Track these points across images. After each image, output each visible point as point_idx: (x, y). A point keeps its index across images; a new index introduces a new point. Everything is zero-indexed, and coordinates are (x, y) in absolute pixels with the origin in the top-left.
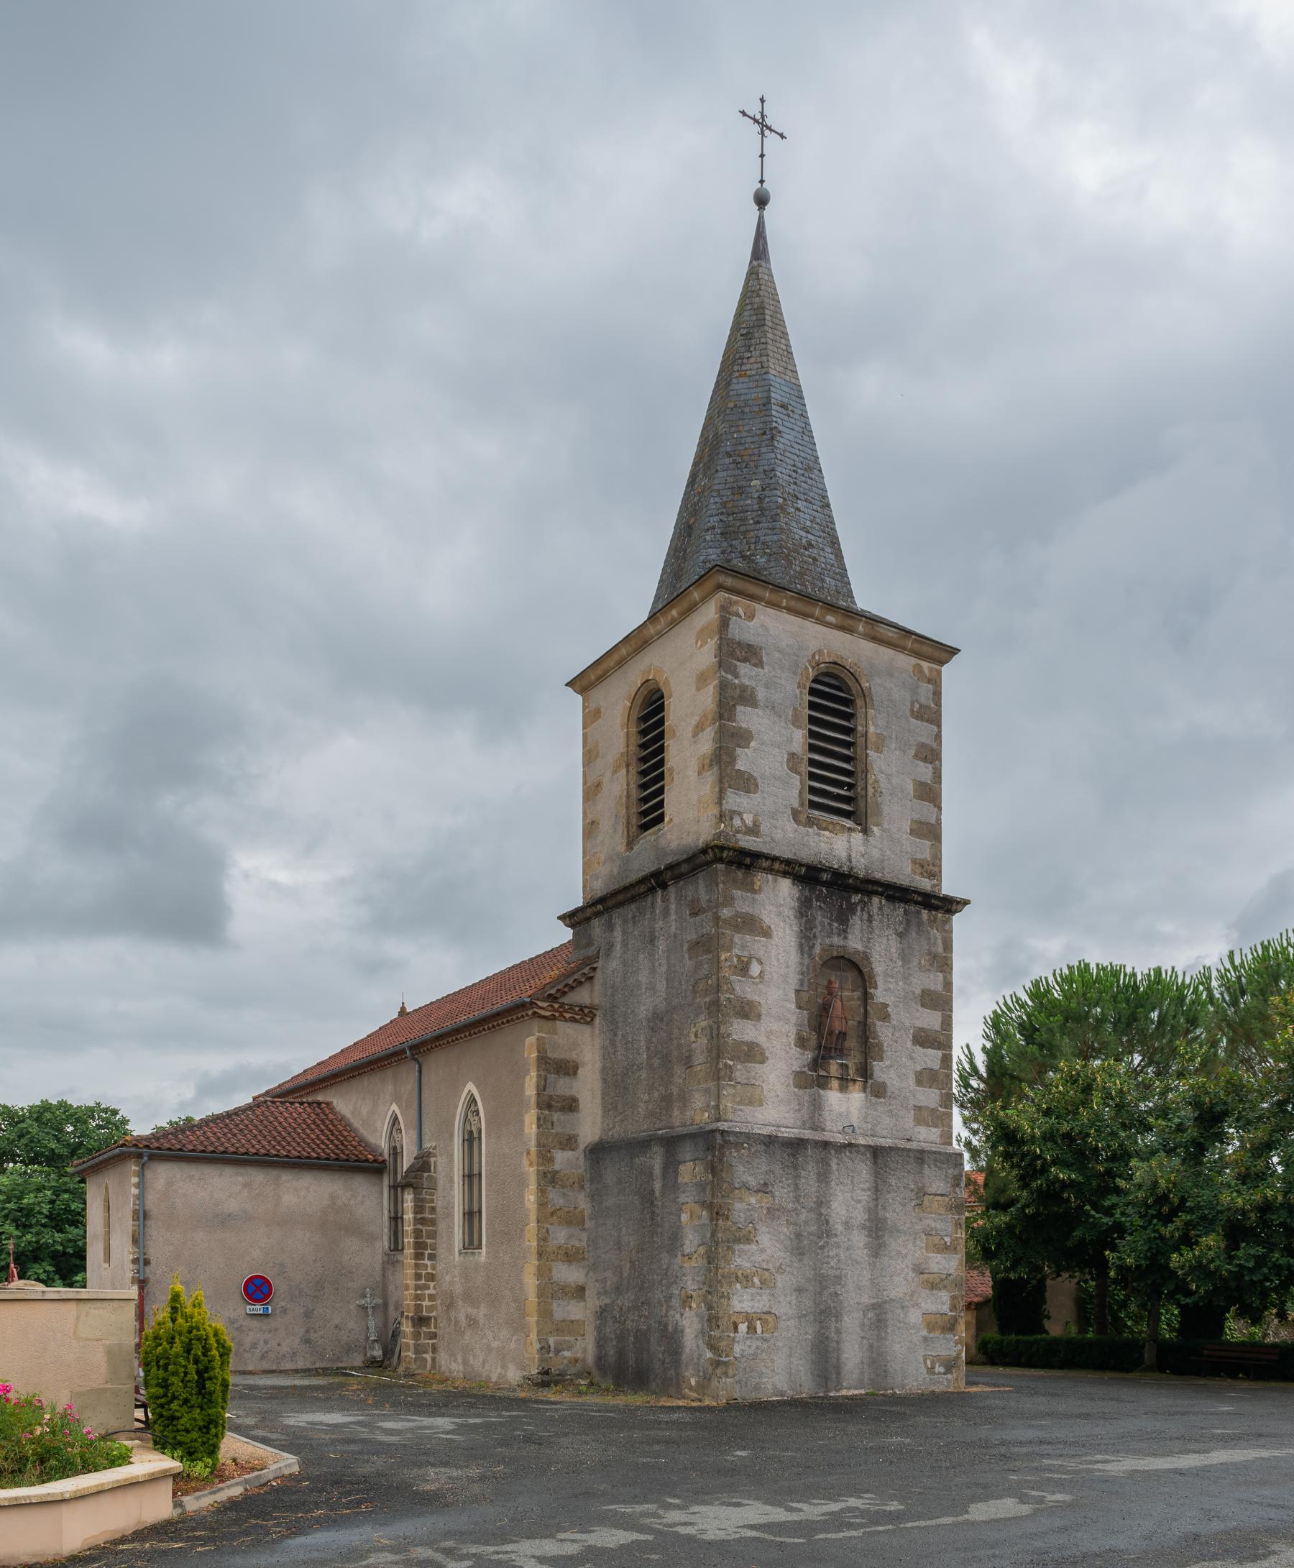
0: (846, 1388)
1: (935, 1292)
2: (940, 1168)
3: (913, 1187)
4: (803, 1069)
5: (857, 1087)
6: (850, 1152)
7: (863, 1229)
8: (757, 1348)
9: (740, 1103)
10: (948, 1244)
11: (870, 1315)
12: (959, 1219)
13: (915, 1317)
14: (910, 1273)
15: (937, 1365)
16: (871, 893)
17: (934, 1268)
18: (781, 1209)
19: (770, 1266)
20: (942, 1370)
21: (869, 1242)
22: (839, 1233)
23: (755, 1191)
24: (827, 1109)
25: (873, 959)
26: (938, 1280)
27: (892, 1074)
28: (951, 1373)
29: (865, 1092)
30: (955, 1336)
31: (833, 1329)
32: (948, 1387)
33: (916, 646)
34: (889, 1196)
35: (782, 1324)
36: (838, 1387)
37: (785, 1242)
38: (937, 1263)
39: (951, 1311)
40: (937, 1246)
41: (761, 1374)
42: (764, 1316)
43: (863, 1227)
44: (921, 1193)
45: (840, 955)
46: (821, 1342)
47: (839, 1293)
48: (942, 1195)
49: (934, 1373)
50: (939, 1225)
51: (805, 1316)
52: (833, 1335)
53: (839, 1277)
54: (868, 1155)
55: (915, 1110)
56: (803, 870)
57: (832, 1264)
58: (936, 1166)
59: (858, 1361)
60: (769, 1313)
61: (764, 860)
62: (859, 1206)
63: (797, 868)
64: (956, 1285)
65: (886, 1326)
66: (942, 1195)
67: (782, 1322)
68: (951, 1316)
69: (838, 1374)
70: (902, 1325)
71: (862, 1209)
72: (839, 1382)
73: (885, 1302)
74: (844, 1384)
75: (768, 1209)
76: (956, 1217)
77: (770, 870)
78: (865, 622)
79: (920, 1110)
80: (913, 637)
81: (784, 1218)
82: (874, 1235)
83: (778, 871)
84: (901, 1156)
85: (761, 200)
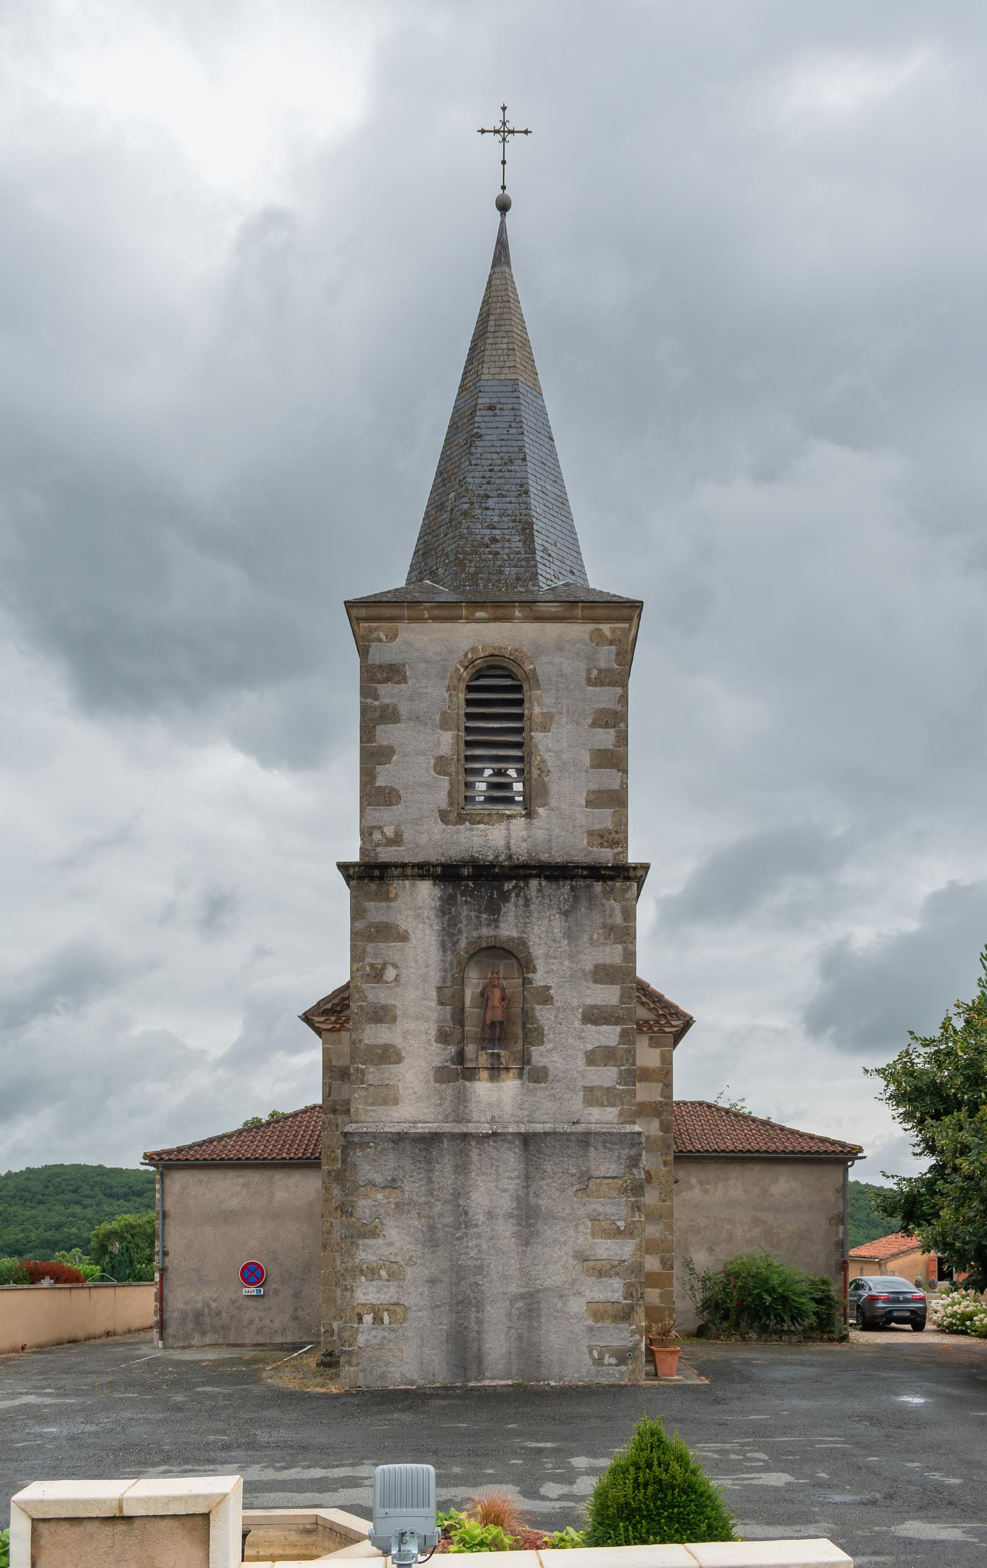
0: (489, 1378)
2: (610, 1149)
3: (574, 1171)
7: (512, 1217)
13: (576, 1306)
14: (571, 1260)
15: (607, 1356)
16: (527, 878)
20: (613, 1361)
24: (474, 1099)
26: (608, 1267)
28: (626, 1364)
30: (630, 1325)
36: (480, 1375)
38: (607, 1249)
39: (625, 1299)
48: (613, 1178)
50: (610, 1209)
56: (439, 870)
59: (504, 1351)
61: (393, 868)
62: (505, 1195)
63: (431, 869)
64: (632, 1272)
65: (540, 1316)
66: (613, 1178)
68: (626, 1305)
69: (480, 1364)
70: (560, 1314)
73: (539, 1291)
77: (404, 877)
78: (520, 606)
85: (503, 206)
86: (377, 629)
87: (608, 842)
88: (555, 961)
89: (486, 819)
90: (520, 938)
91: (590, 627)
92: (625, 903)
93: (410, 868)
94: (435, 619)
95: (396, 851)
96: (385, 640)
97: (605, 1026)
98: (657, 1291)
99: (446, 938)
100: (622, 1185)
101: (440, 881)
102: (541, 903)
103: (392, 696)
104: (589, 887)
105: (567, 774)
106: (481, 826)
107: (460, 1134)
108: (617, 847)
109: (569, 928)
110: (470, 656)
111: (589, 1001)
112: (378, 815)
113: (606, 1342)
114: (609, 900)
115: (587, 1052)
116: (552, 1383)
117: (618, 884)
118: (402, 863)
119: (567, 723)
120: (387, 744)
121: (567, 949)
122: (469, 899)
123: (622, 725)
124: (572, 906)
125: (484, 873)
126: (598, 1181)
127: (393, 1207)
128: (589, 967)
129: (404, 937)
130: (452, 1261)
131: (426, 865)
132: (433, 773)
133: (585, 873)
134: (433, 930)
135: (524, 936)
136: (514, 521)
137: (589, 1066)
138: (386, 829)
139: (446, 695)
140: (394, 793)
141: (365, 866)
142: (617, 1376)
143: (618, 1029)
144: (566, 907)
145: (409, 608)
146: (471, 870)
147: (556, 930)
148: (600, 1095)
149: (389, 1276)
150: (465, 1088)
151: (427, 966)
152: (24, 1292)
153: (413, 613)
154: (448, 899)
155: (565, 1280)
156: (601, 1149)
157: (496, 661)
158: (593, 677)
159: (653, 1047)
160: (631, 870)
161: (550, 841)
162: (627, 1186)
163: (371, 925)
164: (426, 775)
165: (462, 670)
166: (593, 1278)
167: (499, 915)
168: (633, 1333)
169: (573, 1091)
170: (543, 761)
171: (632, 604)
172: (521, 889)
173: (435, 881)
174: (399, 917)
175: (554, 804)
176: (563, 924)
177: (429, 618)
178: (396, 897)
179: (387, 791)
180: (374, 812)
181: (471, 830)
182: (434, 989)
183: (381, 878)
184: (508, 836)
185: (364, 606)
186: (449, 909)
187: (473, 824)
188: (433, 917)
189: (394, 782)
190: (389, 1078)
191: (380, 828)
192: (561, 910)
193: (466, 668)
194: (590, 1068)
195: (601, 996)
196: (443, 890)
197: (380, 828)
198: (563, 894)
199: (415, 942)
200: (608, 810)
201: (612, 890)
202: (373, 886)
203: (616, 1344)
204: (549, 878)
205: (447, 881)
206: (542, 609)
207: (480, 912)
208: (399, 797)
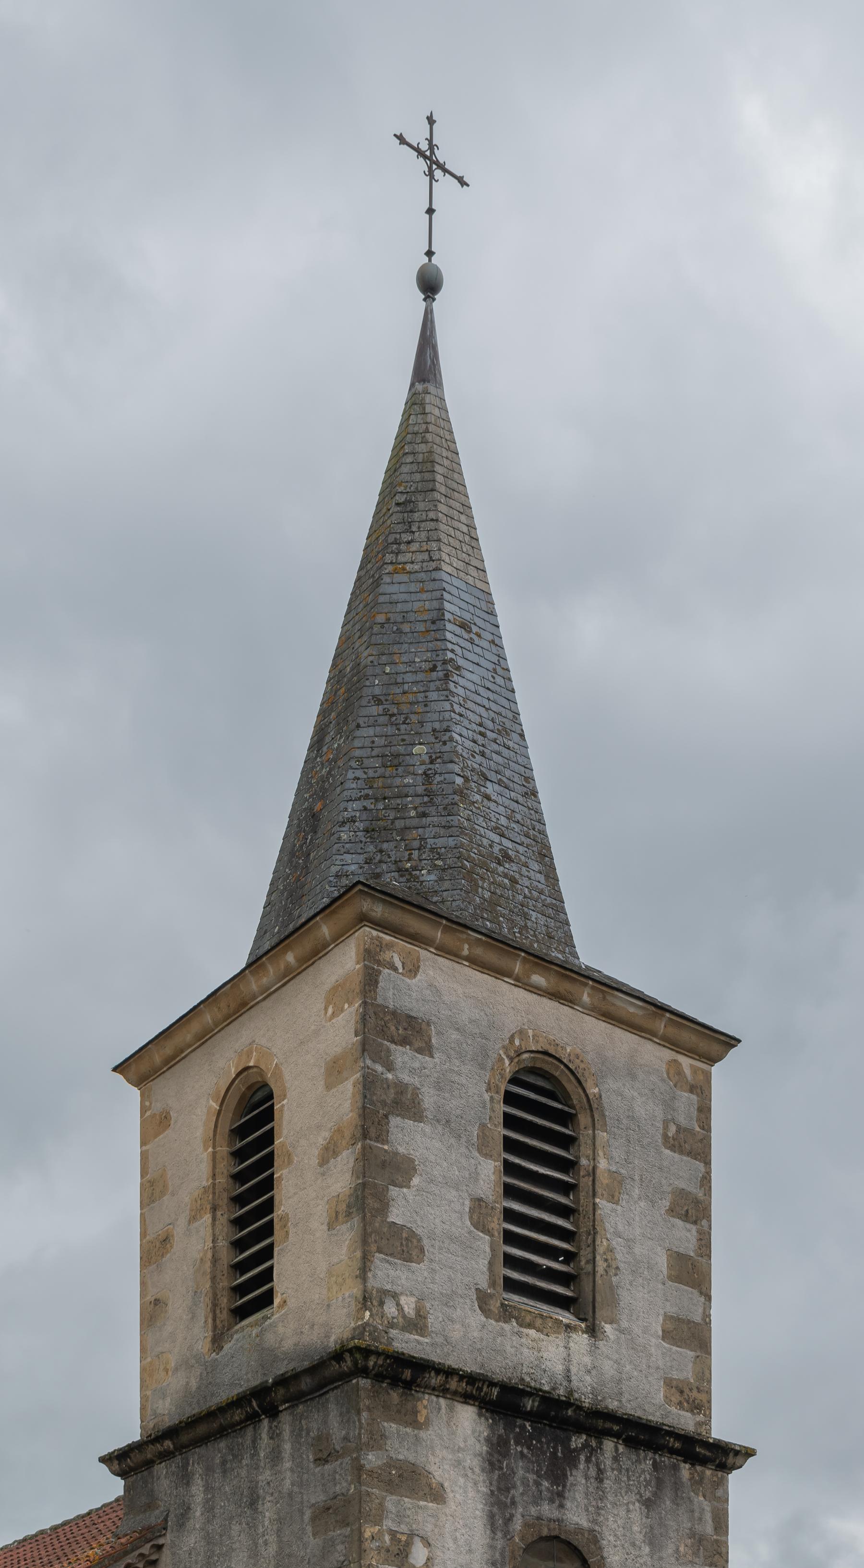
16: (601, 1434)
33: (672, 1031)
56: (495, 1391)
61: (433, 1374)
63: (485, 1389)
77: (443, 1391)
78: (593, 988)
86: (390, 946)
87: (688, 1402)
89: (539, 1322)
90: (591, 1531)
91: (668, 1054)
93: (456, 1379)
94: (475, 962)
95: (418, 1342)
96: (401, 971)
99: (495, 1510)
101: (487, 1410)
102: (618, 1480)
103: (412, 1071)
105: (640, 1280)
106: (532, 1332)
110: (517, 1042)
112: (392, 1273)
118: (449, 1367)
119: (640, 1198)
120: (405, 1152)
121: (648, 1560)
122: (525, 1451)
123: (704, 1222)
124: (655, 1494)
125: (553, 1413)
129: (437, 1495)
131: (480, 1380)
132: (468, 1223)
133: (677, 1445)
134: (478, 1491)
135: (597, 1528)
136: (527, 836)
138: (403, 1300)
139: (487, 1097)
140: (415, 1241)
141: (398, 1358)
145: (446, 929)
146: (536, 1404)
147: (636, 1528)
153: (449, 940)
154: (498, 1444)
157: (547, 1065)
158: (670, 1134)
160: (731, 1455)
161: (619, 1381)
163: (392, 1463)
164: (459, 1224)
165: (507, 1062)
167: (564, 1486)
170: (610, 1250)
172: (593, 1451)
173: (480, 1408)
174: (431, 1458)
175: (624, 1324)
176: (644, 1520)
177: (467, 959)
178: (427, 1424)
179: (404, 1235)
180: (387, 1265)
181: (519, 1335)
183: (408, 1385)
184: (568, 1359)
185: (384, 901)
186: (499, 1461)
187: (521, 1326)
188: (477, 1470)
189: (415, 1222)
191: (395, 1296)
192: (641, 1496)
193: (511, 1059)
196: (491, 1427)
197: (395, 1296)
198: (643, 1471)
199: (454, 1507)
200: (689, 1352)
201: (701, 1481)
202: (395, 1396)
204: (632, 1443)
205: (498, 1413)
206: (619, 1003)
208: (422, 1250)
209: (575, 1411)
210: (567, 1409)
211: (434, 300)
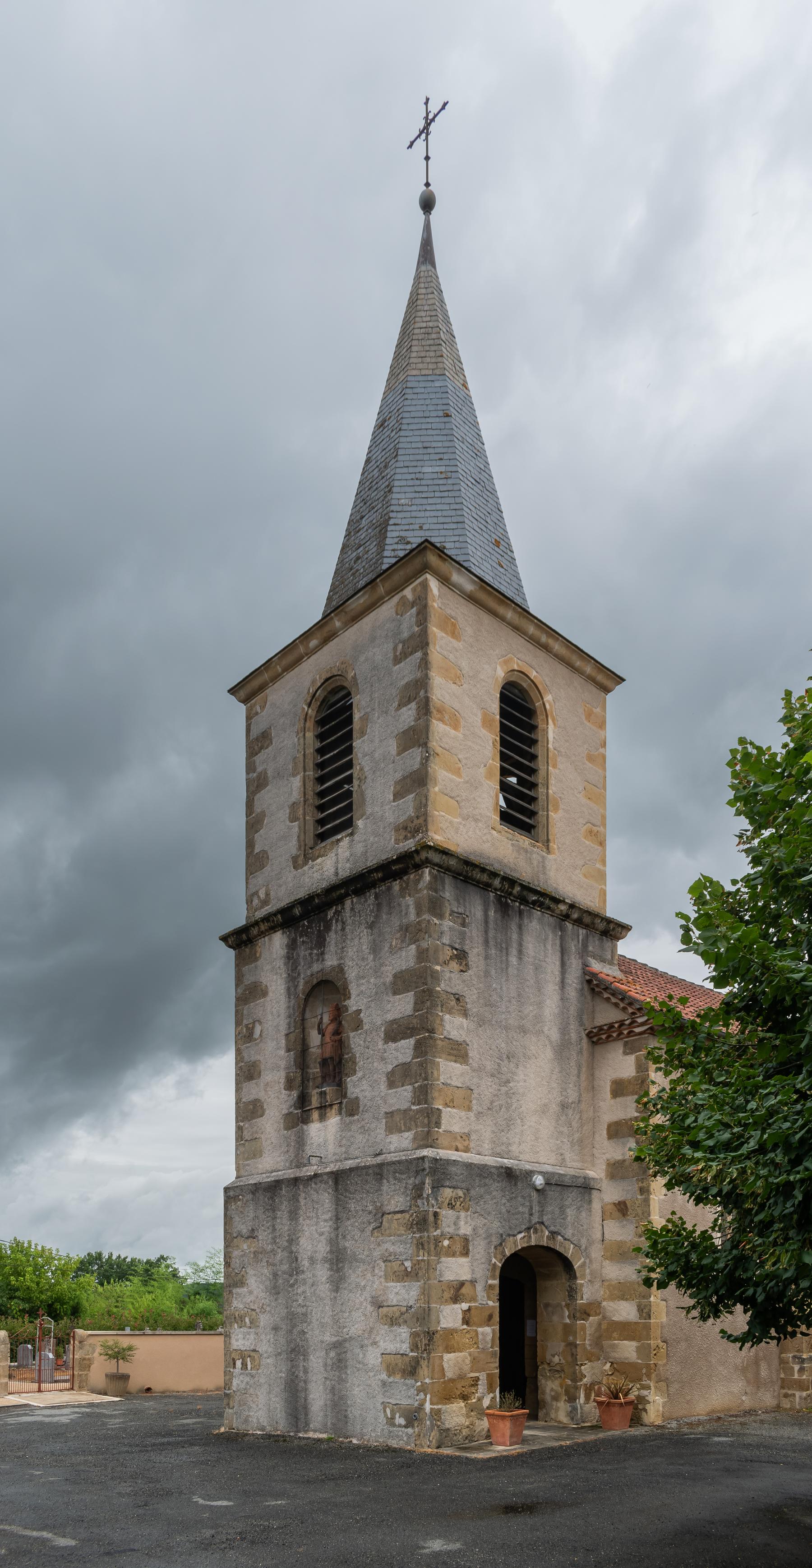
0: (312, 1431)
1: (395, 1328)
2: (400, 1180)
3: (371, 1208)
4: (291, 1110)
5: (333, 1111)
6: (316, 1184)
7: (326, 1262)
8: (247, 1383)
9: (248, 1159)
10: (409, 1270)
11: (332, 1354)
12: (421, 1237)
13: (373, 1358)
14: (369, 1306)
15: (397, 1415)
16: (341, 900)
17: (393, 1299)
18: (263, 1252)
19: (255, 1307)
20: (402, 1421)
21: (331, 1276)
22: (305, 1269)
23: (246, 1238)
24: (309, 1143)
25: (346, 968)
26: (398, 1314)
27: (365, 1085)
28: (413, 1427)
29: (340, 1114)
30: (416, 1381)
31: (301, 1368)
32: (407, 1443)
33: (389, 585)
34: (349, 1223)
35: (264, 1361)
36: (306, 1428)
37: (266, 1283)
38: (397, 1293)
39: (412, 1351)
40: (397, 1274)
41: (250, 1408)
42: (252, 1354)
43: (325, 1260)
44: (380, 1214)
45: (319, 980)
46: (292, 1380)
47: (306, 1330)
48: (402, 1212)
49: (394, 1425)
50: (398, 1248)
51: (280, 1354)
52: (301, 1374)
53: (305, 1315)
54: (330, 1183)
55: (386, 1118)
56: (279, 916)
57: (300, 1301)
58: (395, 1179)
59: (322, 1403)
60: (254, 1351)
61: (252, 929)
62: (323, 1238)
63: (275, 919)
64: (418, 1319)
65: (346, 1367)
66: (402, 1212)
67: (264, 1360)
68: (413, 1357)
69: (306, 1415)
70: (361, 1366)
71: (324, 1241)
72: (307, 1424)
73: (345, 1340)
74: (311, 1426)
75: (254, 1253)
76: (417, 1235)
77: (262, 934)
78: (336, 615)
79: (392, 1116)
80: (378, 580)
81: (265, 1260)
82: (335, 1268)
83: (266, 930)
84: (360, 1176)
85: (427, 204)
88: (364, 981)
92: (417, 895)
97: (403, 1041)
98: (634, 1344)
100: (409, 1220)
104: (389, 889)
107: (292, 1179)
108: (418, 835)
109: (374, 940)
111: (390, 1017)
113: (396, 1399)
114: (404, 897)
115: (388, 1073)
116: (355, 1441)
117: (412, 876)
126: (390, 1216)
127: (252, 1256)
128: (389, 979)
130: (287, 1308)
137: (390, 1089)
142: (405, 1439)
143: (412, 1041)
144: (372, 919)
146: (300, 909)
148: (398, 1119)
149: (251, 1323)
150: (302, 1130)
151: (279, 1016)
152: (169, 1337)
155: (365, 1329)
156: (393, 1182)
159: (627, 1054)
160: (415, 855)
162: (413, 1220)
166: (386, 1327)
168: (419, 1391)
169: (378, 1119)
171: (419, 549)
182: (284, 1038)
190: (257, 1132)
194: (390, 1091)
195: (399, 1008)
203: (405, 1402)
204: (359, 892)
207: (311, 949)
209: (318, 898)
210: (314, 900)
211: (430, 214)
